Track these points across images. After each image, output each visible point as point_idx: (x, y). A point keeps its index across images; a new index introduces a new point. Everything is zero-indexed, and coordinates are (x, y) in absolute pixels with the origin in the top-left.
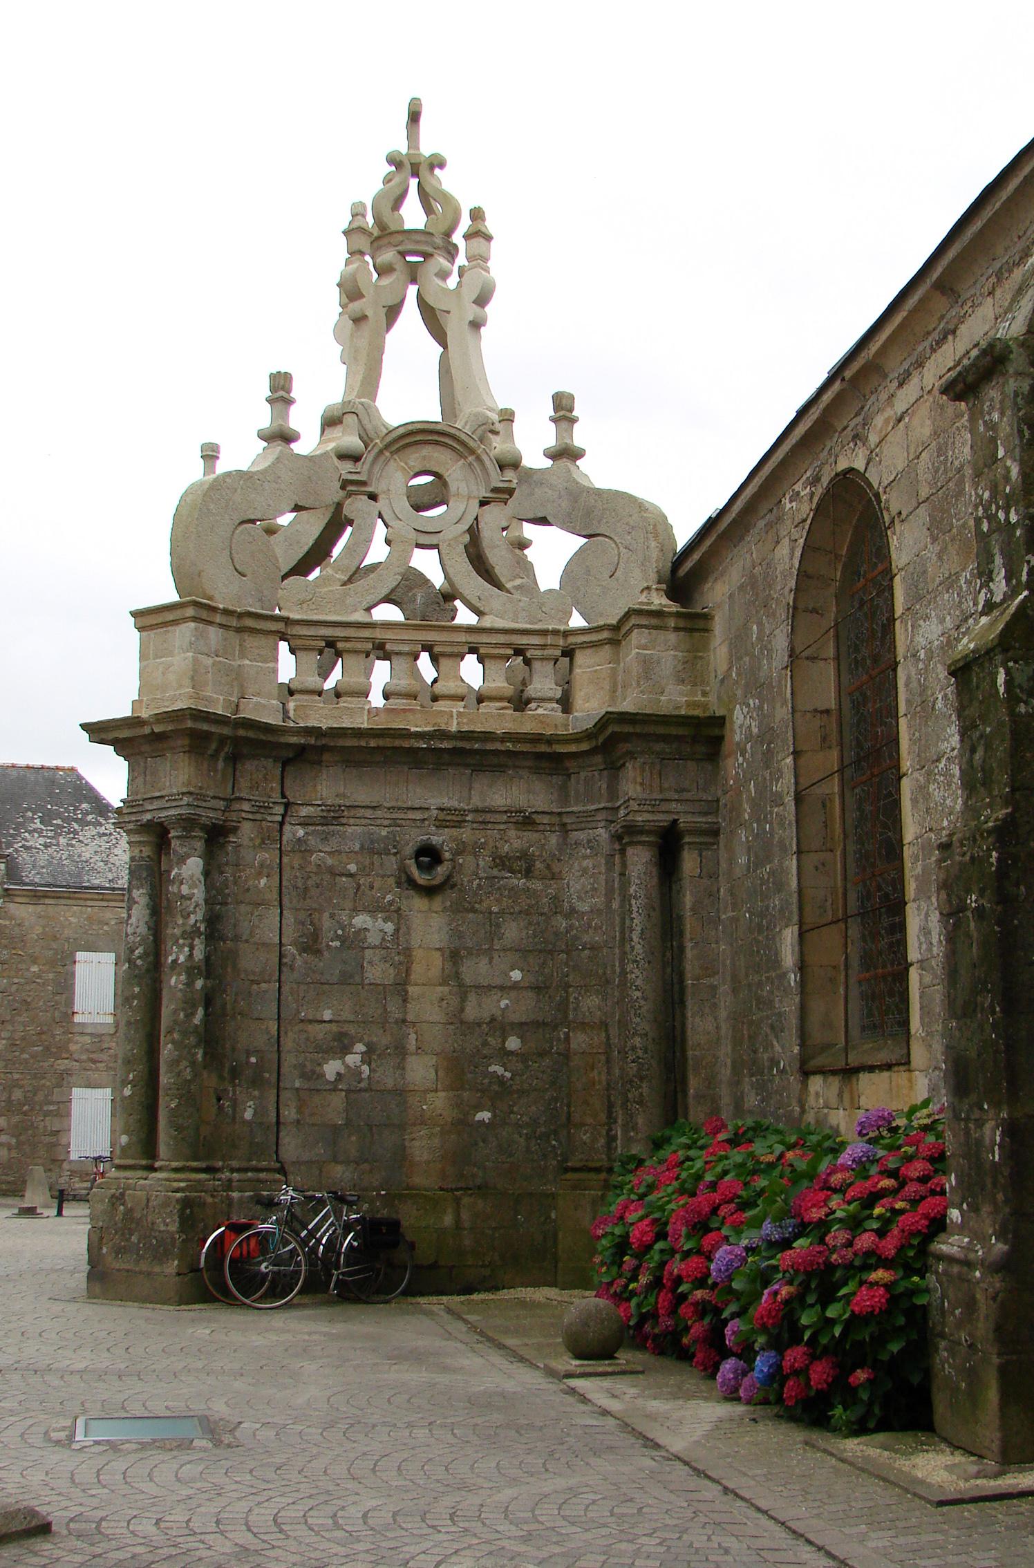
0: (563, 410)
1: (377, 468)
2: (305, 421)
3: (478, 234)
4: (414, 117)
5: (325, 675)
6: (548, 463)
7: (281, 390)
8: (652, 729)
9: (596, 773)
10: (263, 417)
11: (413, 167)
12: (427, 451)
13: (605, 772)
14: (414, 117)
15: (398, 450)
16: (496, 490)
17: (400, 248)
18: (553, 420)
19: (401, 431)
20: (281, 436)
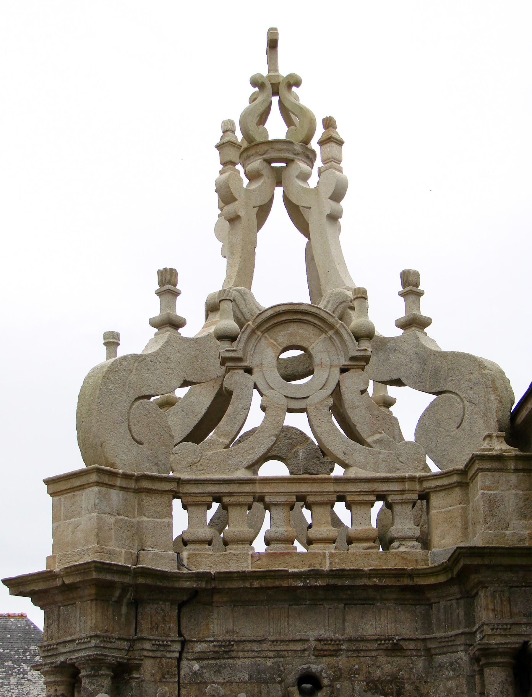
2: (191, 309)
3: (331, 140)
4: (273, 44)
7: (168, 284)
10: (154, 308)
11: (274, 87)
14: (273, 44)
16: (353, 358)
17: (265, 156)
18: (402, 294)
19: (270, 313)
20: (170, 323)
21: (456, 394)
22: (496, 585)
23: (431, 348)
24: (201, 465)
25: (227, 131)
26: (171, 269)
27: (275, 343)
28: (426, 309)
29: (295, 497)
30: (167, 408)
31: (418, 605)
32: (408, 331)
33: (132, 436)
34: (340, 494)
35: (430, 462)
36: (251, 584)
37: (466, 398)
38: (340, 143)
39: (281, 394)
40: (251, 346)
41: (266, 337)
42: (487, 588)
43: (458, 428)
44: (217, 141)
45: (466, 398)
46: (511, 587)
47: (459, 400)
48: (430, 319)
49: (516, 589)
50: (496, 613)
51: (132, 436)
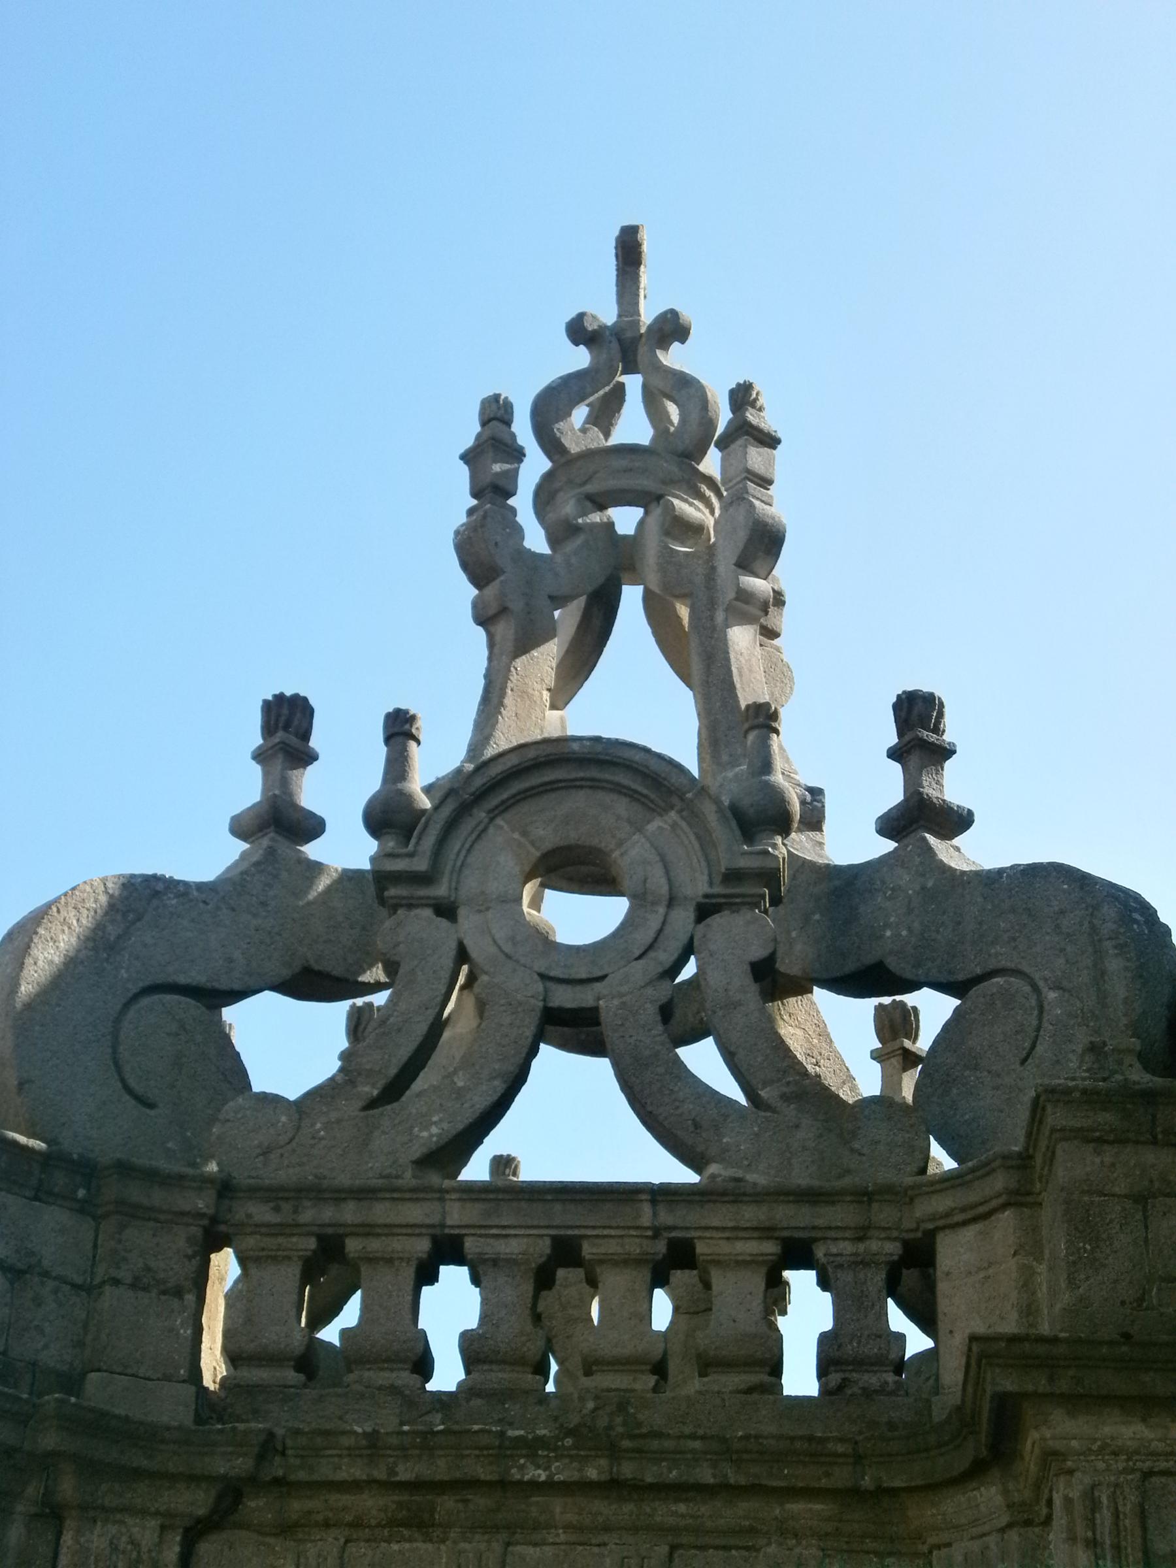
0: (919, 728)
1: (455, 845)
2: (339, 789)
3: (749, 433)
4: (629, 250)
5: (325, 1313)
6: (889, 845)
7: (288, 728)
8: (409, 1231)
9: (992, 1540)
10: (247, 788)
11: (624, 346)
12: (577, 801)
13: (1013, 1536)
14: (629, 250)
15: (504, 807)
16: (733, 876)
17: (589, 488)
18: (895, 754)
19: (513, 760)
20: (280, 824)
21: (1017, 972)
22: (1101, 1465)
23: (953, 865)
24: (294, 1151)
25: (490, 420)
26: (296, 697)
27: (523, 840)
28: (954, 785)
29: (548, 1241)
30: (98, 918)
31: (890, 1554)
32: (906, 841)
33: (123, 1081)
34: (673, 1234)
35: (937, 1151)
36: (392, 1472)
37: (1046, 980)
38: (771, 441)
39: (531, 968)
40: (457, 848)
41: (501, 828)
42: (1071, 1472)
43: (1023, 1062)
44: (468, 442)
45: (1046, 980)
46: (1148, 1475)
47: (1027, 989)
48: (970, 813)
49: (1163, 1480)
50: (1099, 1551)
51: (123, 1081)
